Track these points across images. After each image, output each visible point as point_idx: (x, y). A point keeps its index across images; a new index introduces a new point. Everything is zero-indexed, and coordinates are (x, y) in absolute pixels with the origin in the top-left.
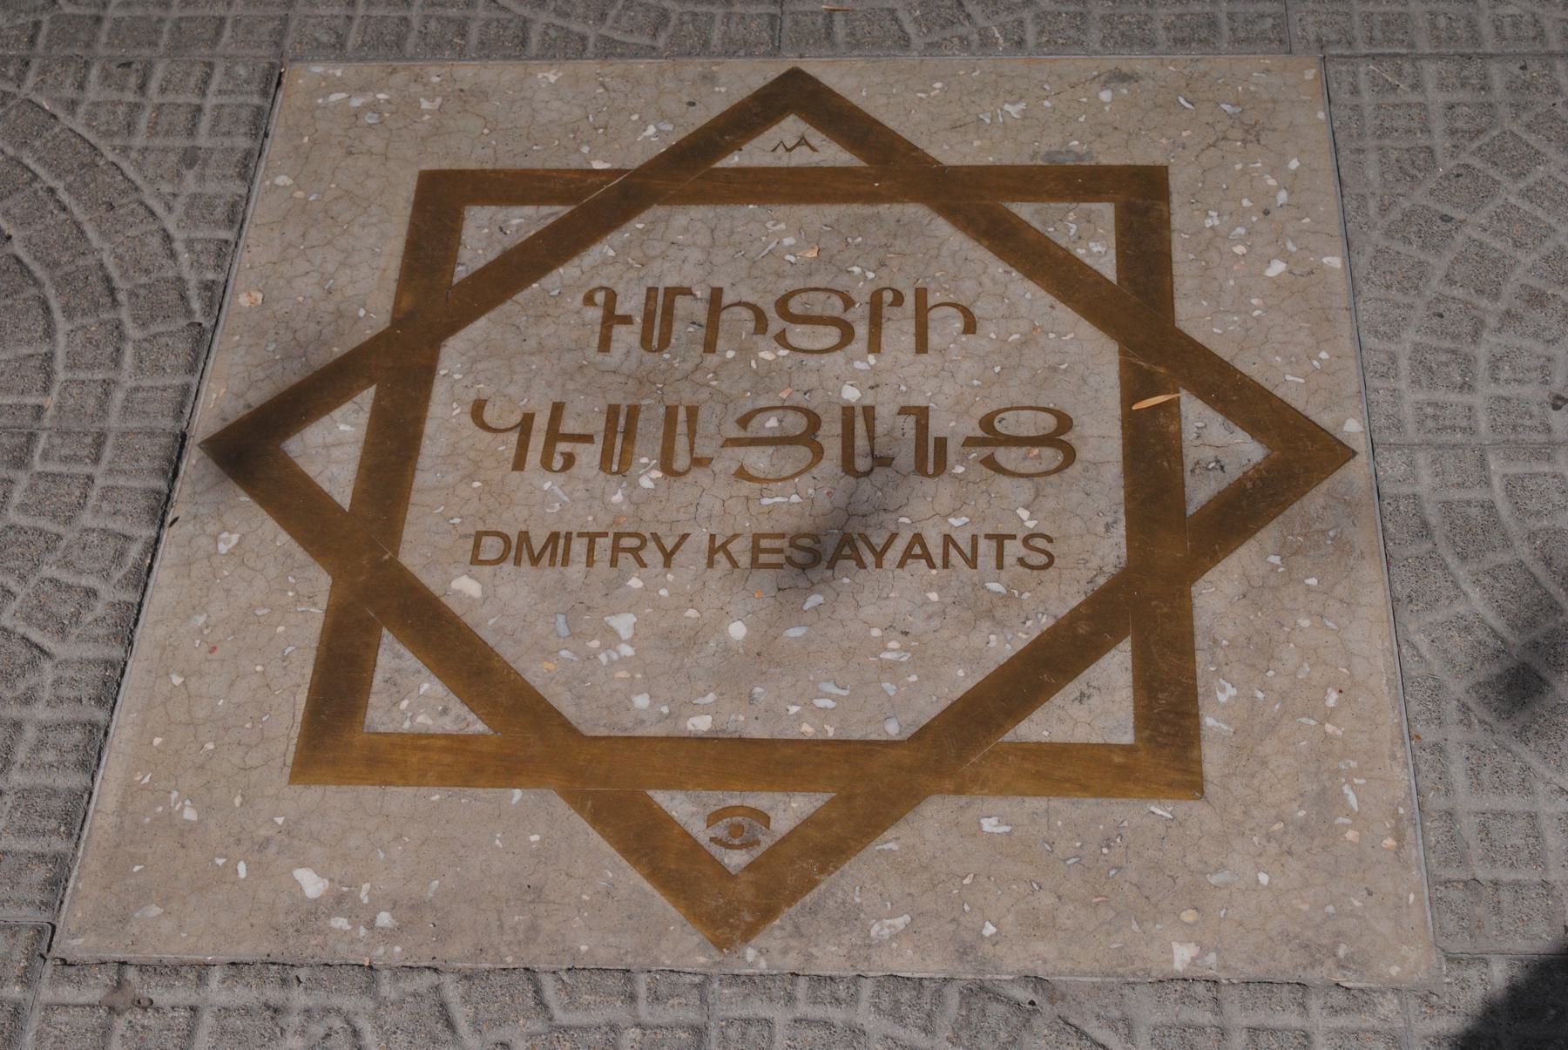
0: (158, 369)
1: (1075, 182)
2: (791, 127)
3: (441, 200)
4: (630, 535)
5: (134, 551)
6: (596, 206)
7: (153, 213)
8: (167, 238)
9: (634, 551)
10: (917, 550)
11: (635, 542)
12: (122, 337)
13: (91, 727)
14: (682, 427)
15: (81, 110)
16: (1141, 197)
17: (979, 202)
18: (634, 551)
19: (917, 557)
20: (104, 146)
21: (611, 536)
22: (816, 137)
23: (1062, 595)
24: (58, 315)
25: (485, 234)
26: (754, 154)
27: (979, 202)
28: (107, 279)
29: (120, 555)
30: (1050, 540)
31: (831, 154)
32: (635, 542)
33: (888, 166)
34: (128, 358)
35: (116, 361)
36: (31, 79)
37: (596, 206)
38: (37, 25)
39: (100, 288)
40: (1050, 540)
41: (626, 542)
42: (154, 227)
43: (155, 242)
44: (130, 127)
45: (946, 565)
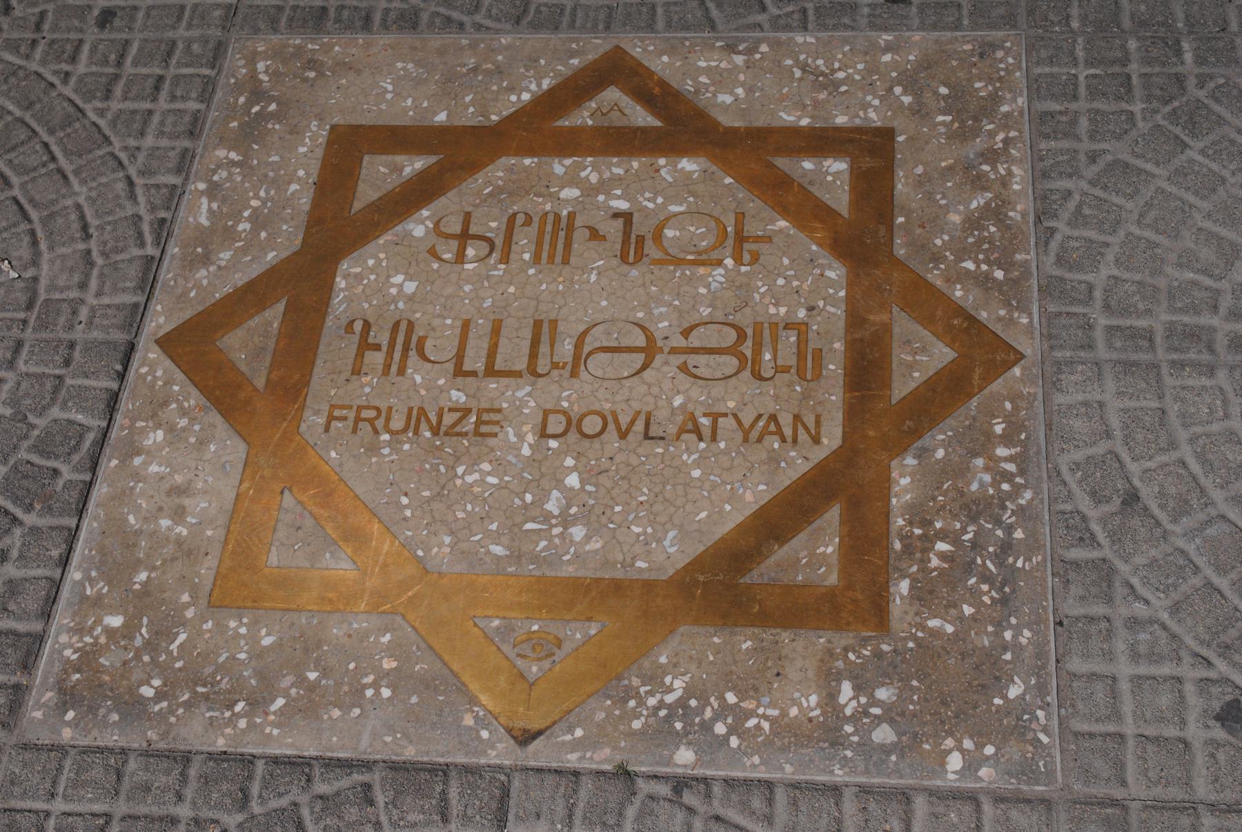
0: (116, 290)
1: (822, 141)
2: (612, 94)
3: (349, 146)
4: (367, 407)
5: (90, 437)
6: (458, 152)
7: (120, 163)
8: (130, 183)
9: (371, 421)
10: (772, 428)
11: (373, 414)
12: (91, 264)
13: (17, 687)
14: (545, 338)
15: (73, 80)
16: (872, 150)
17: (754, 154)
18: (371, 421)
19: (771, 433)
20: (88, 108)
21: (355, 408)
22: (626, 101)
23: (798, 463)
24: (43, 246)
25: (382, 174)
26: (583, 117)
27: (754, 154)
28: (82, 217)
29: (158, 48)
30: (760, 416)
31: (642, 117)
32: (373, 414)
33: (681, 125)
34: (94, 283)
35: (83, 286)
36: (38, 54)
37: (458, 152)
38: (43, 14)
39: (76, 226)
40: (760, 416)
41: (366, 414)
42: (121, 174)
43: (121, 187)
44: (108, 95)
45: (795, 441)
